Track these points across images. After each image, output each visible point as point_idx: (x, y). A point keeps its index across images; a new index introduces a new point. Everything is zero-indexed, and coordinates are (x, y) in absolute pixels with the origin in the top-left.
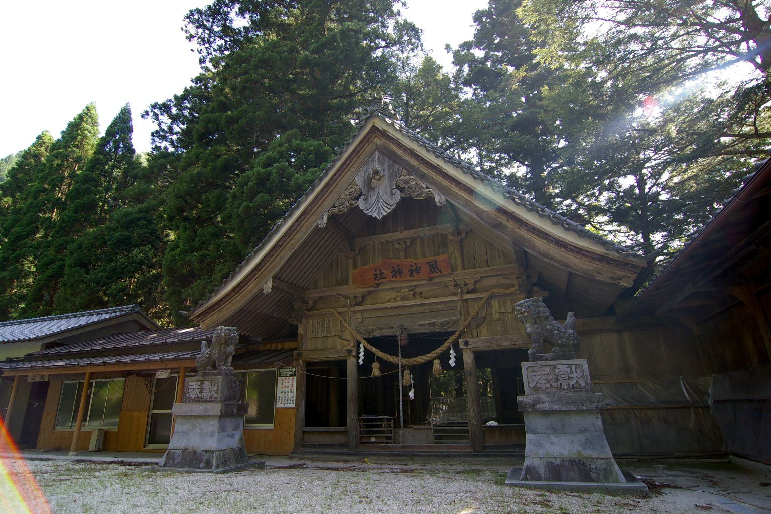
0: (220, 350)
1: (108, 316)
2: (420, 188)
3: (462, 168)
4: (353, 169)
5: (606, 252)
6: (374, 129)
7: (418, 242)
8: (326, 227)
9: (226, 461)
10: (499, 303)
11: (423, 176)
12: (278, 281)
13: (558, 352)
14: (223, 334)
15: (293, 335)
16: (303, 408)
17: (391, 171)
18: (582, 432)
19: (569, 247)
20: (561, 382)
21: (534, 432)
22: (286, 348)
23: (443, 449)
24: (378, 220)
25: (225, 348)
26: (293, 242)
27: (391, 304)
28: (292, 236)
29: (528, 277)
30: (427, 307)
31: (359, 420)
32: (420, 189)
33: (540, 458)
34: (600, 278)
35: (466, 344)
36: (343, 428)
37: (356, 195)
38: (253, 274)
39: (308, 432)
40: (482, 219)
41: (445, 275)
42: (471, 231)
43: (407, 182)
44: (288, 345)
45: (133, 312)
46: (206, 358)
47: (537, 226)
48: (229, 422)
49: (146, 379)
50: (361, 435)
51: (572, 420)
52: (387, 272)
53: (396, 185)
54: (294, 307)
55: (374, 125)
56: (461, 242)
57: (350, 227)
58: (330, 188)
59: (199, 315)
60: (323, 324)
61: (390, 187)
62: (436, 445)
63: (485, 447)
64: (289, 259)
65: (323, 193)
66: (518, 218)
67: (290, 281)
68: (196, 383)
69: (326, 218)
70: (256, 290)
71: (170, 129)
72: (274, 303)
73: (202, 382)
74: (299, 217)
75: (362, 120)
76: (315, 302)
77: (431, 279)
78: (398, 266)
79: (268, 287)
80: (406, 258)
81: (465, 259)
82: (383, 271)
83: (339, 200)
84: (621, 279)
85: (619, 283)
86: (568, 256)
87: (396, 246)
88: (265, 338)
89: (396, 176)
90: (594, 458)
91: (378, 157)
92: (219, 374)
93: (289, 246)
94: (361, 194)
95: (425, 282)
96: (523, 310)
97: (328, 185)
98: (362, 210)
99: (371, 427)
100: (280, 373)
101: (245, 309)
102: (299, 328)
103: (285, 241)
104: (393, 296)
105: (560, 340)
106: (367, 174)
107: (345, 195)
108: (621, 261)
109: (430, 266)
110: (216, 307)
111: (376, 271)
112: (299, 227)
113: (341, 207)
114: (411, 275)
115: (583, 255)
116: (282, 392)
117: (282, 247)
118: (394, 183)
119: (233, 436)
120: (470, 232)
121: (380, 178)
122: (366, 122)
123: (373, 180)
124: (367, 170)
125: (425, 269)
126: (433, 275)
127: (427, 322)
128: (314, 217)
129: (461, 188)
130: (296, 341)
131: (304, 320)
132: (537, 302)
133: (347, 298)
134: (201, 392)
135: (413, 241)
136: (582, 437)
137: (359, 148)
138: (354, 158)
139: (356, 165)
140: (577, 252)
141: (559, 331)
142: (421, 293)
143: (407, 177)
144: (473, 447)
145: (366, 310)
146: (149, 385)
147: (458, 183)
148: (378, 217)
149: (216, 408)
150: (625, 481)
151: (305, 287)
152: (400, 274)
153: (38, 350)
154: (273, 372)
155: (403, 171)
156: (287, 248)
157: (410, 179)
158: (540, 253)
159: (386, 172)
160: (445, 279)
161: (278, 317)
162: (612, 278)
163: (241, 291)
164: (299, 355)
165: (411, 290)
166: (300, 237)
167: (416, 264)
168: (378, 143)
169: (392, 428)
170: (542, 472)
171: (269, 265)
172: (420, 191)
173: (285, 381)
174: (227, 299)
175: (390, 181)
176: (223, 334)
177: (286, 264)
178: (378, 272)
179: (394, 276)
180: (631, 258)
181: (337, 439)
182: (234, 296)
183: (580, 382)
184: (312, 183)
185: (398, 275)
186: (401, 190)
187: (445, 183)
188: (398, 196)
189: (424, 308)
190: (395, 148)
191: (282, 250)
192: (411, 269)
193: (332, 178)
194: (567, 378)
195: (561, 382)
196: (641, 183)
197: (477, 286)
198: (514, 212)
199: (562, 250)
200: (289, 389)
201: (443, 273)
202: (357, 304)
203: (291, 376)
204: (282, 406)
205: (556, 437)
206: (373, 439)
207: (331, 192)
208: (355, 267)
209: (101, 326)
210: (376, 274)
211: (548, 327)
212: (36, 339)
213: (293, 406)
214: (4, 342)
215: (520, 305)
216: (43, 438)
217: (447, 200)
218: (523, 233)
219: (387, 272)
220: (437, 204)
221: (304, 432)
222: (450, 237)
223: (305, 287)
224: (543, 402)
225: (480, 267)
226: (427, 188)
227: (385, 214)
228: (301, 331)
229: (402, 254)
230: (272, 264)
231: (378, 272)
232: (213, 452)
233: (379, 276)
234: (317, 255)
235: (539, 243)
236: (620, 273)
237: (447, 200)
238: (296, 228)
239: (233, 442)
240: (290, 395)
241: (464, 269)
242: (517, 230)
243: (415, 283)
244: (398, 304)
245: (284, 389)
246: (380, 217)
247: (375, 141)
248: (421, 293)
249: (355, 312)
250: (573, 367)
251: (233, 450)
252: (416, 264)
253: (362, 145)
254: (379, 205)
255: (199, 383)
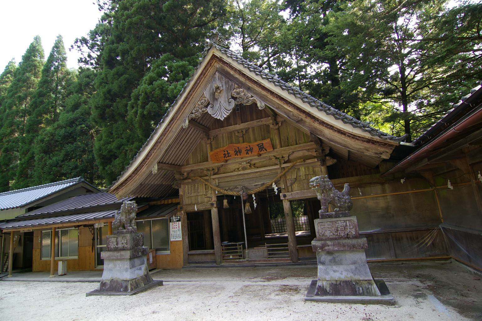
0: (126, 217)
1: (68, 185)
2: (247, 97)
3: (274, 82)
4: (202, 86)
5: (371, 137)
6: (214, 57)
7: (251, 131)
8: (189, 127)
9: (137, 285)
10: (305, 169)
11: (249, 89)
12: (161, 165)
13: (338, 211)
14: (127, 207)
15: (176, 194)
16: (187, 241)
17: (227, 86)
18: (354, 263)
19: (347, 134)
20: (339, 232)
21: (323, 263)
22: (174, 202)
23: (274, 261)
24: (221, 121)
25: (129, 215)
26: (167, 139)
27: (236, 173)
28: (166, 135)
29: (323, 150)
30: (259, 173)
31: (222, 245)
32: (247, 98)
33: (327, 281)
34: (368, 154)
35: (285, 196)
36: (212, 251)
37: (205, 104)
38: (144, 164)
39: (191, 255)
40: (289, 117)
41: (269, 152)
42: (285, 121)
43: (238, 93)
44: (175, 201)
45: (80, 182)
46: (118, 222)
47: (325, 120)
48: (137, 261)
49: (90, 227)
50: (224, 255)
51: (346, 256)
52: (232, 152)
53: (231, 96)
54: (176, 178)
55: (213, 55)
56: (278, 129)
57: (204, 125)
58: (188, 100)
59: (114, 190)
60: (195, 187)
61: (228, 98)
62: (269, 259)
63: (299, 259)
64: (166, 150)
65: (183, 105)
66: (312, 116)
67: (170, 163)
68: (113, 239)
69: (187, 122)
70: (147, 172)
71: (89, 56)
72: (161, 176)
73: (117, 238)
74: (170, 122)
75: (205, 51)
76: (188, 174)
77: (260, 155)
78: (238, 148)
79: (155, 169)
80: (244, 142)
81: (282, 141)
82: (229, 152)
83: (194, 108)
84: (382, 154)
85: (380, 156)
86: (346, 140)
87: (237, 134)
88: (155, 202)
89: (231, 90)
90: (361, 280)
91: (218, 77)
92: (127, 233)
93: (165, 141)
94: (209, 104)
95: (257, 157)
96: (315, 185)
97: (186, 98)
98: (211, 115)
99: (229, 250)
100: (171, 220)
101: (143, 183)
102: (180, 191)
103: (162, 139)
104: (237, 167)
105: (339, 203)
106: (212, 89)
107: (198, 105)
108: (381, 142)
109: (259, 147)
110: (124, 184)
111: (225, 152)
112: (170, 129)
113: (196, 113)
114: (247, 153)
115: (356, 139)
116: (173, 231)
117: (161, 142)
118: (230, 94)
119: (140, 269)
120: (284, 122)
121: (220, 93)
122: (208, 52)
123: (216, 93)
124: (212, 86)
125: (256, 149)
126: (261, 153)
127: (260, 183)
128: (179, 121)
129: (274, 96)
130: (179, 198)
131: (182, 186)
132: (324, 179)
133: (208, 170)
134: (117, 244)
135: (247, 130)
136: (353, 267)
137: (204, 72)
138: (202, 79)
139: (204, 82)
140: (352, 137)
141: (338, 197)
142: (254, 164)
143: (238, 90)
144: (291, 260)
145: (220, 178)
146: (92, 231)
147: (272, 93)
148: (221, 119)
149: (128, 254)
150: (380, 294)
151: (181, 165)
152: (240, 153)
153: (24, 212)
154: (167, 220)
155: (236, 85)
156: (164, 143)
157: (240, 91)
158: (328, 139)
159: (224, 87)
160: (270, 154)
161: (166, 184)
162: (376, 153)
163: (138, 173)
164: (181, 208)
165: (248, 163)
166: (171, 136)
167: (250, 146)
168: (218, 66)
169: (242, 250)
170: (328, 289)
171: (154, 155)
172: (247, 100)
173: (174, 224)
174: (130, 179)
175: (227, 93)
176: (127, 207)
177: (165, 154)
178: (226, 153)
179: (236, 154)
180: (389, 140)
181: (209, 258)
182: (134, 176)
183: (352, 232)
184: (180, 93)
185: (238, 154)
186: (235, 98)
187: (264, 93)
188: (233, 103)
189: (257, 174)
190: (228, 69)
191: (161, 145)
192: (247, 150)
193: (189, 93)
194: (343, 229)
195: (339, 232)
196: (402, 70)
197: (290, 158)
198: (310, 112)
199: (343, 136)
200: (177, 229)
201: (268, 151)
202: (215, 174)
203: (178, 221)
204: (174, 240)
205: (337, 267)
206: (231, 257)
207: (189, 103)
208: (212, 150)
209: (61, 193)
210: (225, 154)
211: (331, 195)
212: (22, 207)
213: (181, 239)
214: (2, 210)
215: (312, 182)
216: (35, 265)
217: (265, 104)
218: (316, 125)
219: (232, 152)
220: (259, 108)
221: (189, 254)
222: (271, 126)
223: (181, 165)
224: (328, 246)
225: (292, 145)
226: (252, 97)
227: (225, 116)
228: (181, 193)
229: (241, 139)
230: (156, 154)
231: (226, 153)
232: (128, 281)
233: (227, 155)
234: (186, 144)
235: (327, 132)
236: (381, 149)
237: (265, 104)
238: (169, 130)
239: (140, 272)
240: (178, 233)
241: (281, 147)
242: (313, 124)
243: (250, 158)
244: (240, 172)
245: (174, 230)
246: (222, 119)
247: (215, 65)
248: (254, 164)
249: (214, 179)
250: (348, 222)
251: (142, 277)
252: (250, 146)
253: (206, 69)
254: (221, 110)
255: (115, 239)
